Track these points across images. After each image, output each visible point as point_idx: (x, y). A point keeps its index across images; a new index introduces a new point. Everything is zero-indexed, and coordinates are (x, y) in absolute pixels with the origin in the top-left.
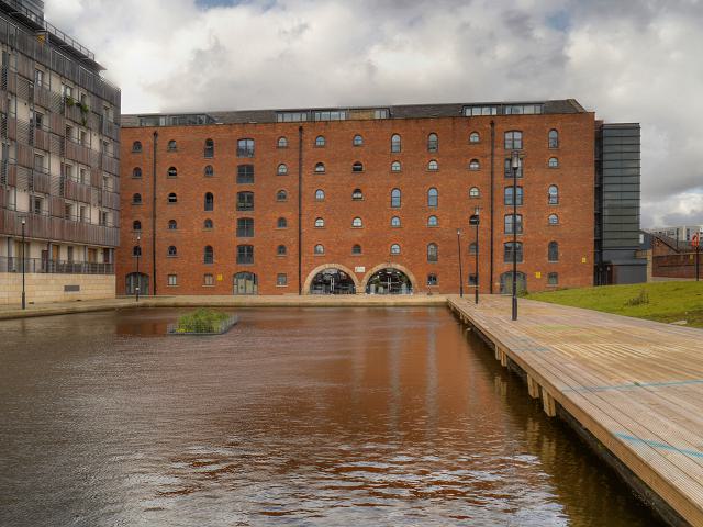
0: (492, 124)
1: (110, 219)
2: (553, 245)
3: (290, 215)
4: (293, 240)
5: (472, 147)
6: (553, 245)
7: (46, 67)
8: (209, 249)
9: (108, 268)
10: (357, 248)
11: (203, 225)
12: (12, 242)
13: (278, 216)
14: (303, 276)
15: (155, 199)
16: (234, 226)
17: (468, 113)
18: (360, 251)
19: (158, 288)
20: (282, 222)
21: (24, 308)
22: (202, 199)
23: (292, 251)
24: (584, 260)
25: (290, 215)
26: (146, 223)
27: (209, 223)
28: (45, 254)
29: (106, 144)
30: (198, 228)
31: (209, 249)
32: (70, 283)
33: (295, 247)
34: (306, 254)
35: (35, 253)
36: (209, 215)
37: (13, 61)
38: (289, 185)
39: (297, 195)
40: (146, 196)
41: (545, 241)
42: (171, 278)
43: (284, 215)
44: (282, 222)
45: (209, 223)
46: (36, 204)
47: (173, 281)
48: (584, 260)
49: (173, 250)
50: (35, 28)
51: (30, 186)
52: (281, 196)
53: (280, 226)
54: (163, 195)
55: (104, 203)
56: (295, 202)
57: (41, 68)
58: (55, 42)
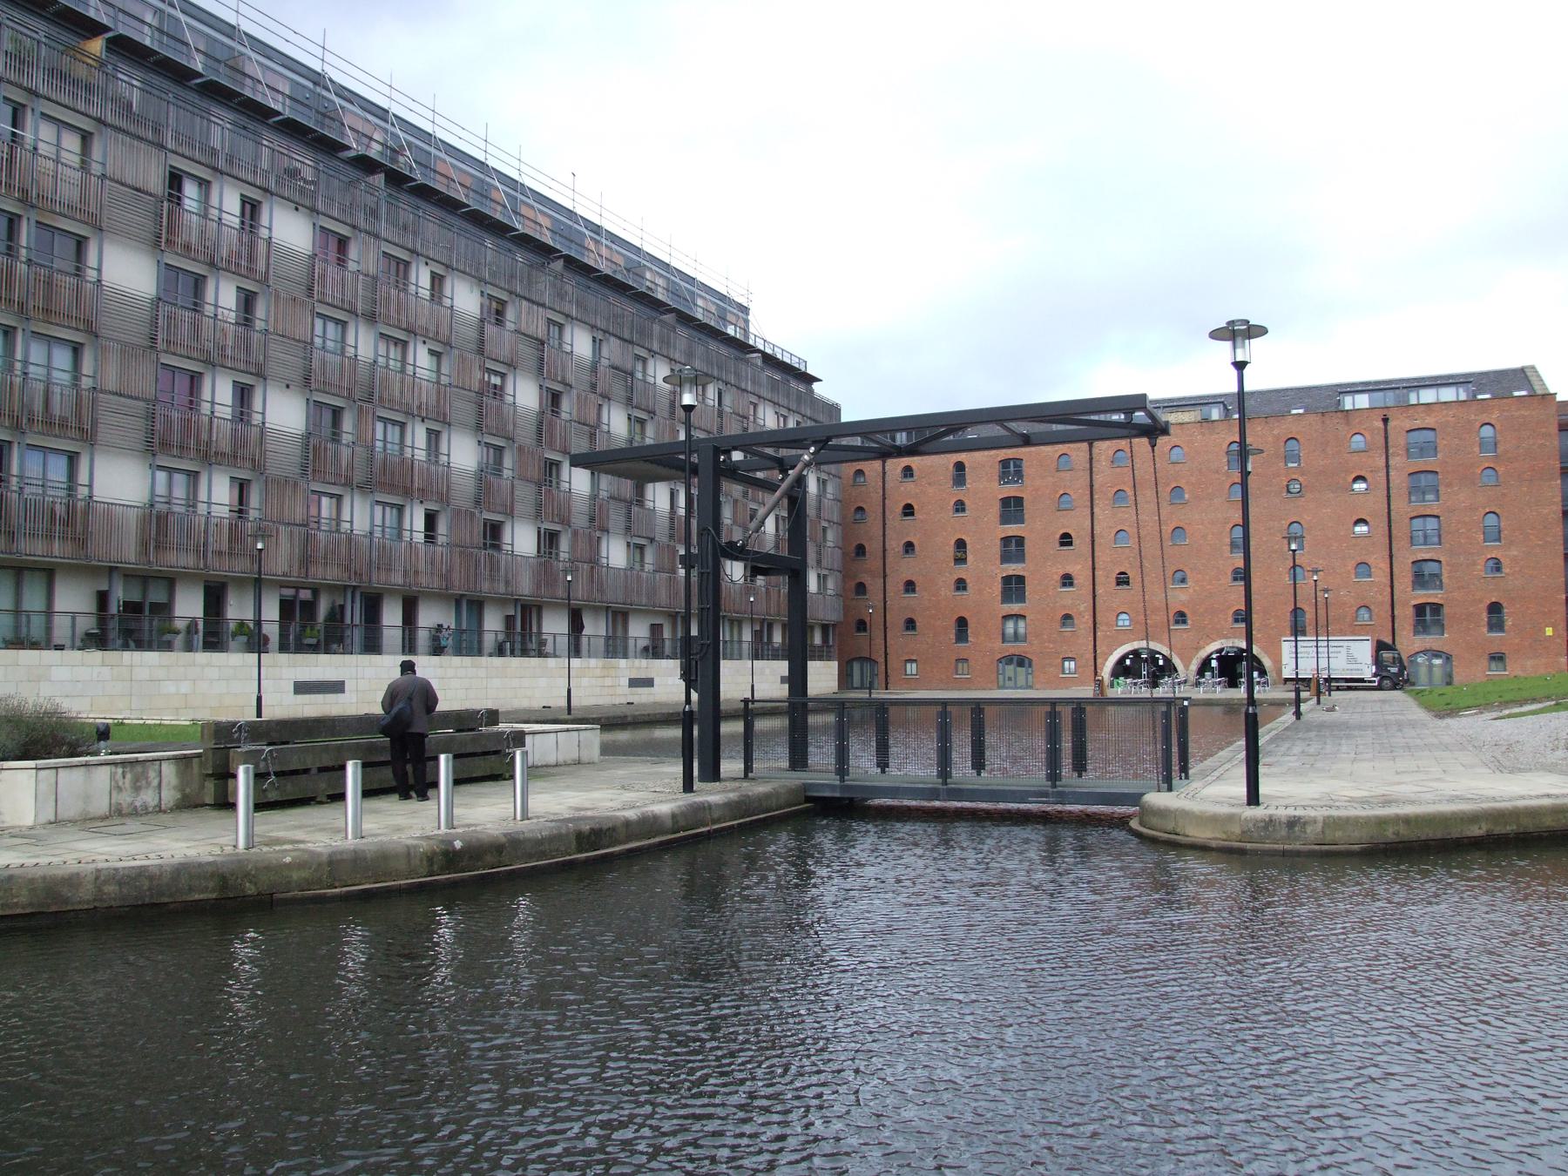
0: (1385, 420)
1: (830, 584)
2: (1495, 609)
3: (1080, 571)
4: (1084, 607)
5: (1355, 458)
6: (1495, 609)
7: (759, 397)
8: (962, 623)
9: (829, 652)
10: (1181, 617)
11: (953, 587)
12: (115, 575)
13: (1062, 572)
14: (1099, 661)
15: (884, 550)
16: (997, 588)
17: (1348, 403)
18: (1184, 622)
19: (891, 680)
20: (1067, 580)
21: (569, 713)
22: (950, 549)
23: (1083, 622)
24: (1549, 631)
25: (1080, 571)
26: (874, 585)
27: (961, 585)
28: (757, 635)
29: (642, 422)
30: (947, 590)
31: (962, 623)
32: (646, 690)
33: (1088, 617)
34: (1104, 628)
35: (493, 622)
36: (960, 572)
37: (727, 400)
38: (1076, 524)
39: (1088, 539)
40: (873, 547)
41: (1480, 601)
42: (908, 665)
43: (1069, 569)
44: (1067, 580)
45: (961, 585)
46: (549, 540)
47: (912, 668)
48: (1549, 631)
49: (910, 624)
50: (743, 347)
51: (628, 529)
52: (1066, 540)
53: (1064, 585)
54: (895, 546)
55: (824, 563)
56: (1087, 549)
57: (643, 353)
58: (770, 361)
